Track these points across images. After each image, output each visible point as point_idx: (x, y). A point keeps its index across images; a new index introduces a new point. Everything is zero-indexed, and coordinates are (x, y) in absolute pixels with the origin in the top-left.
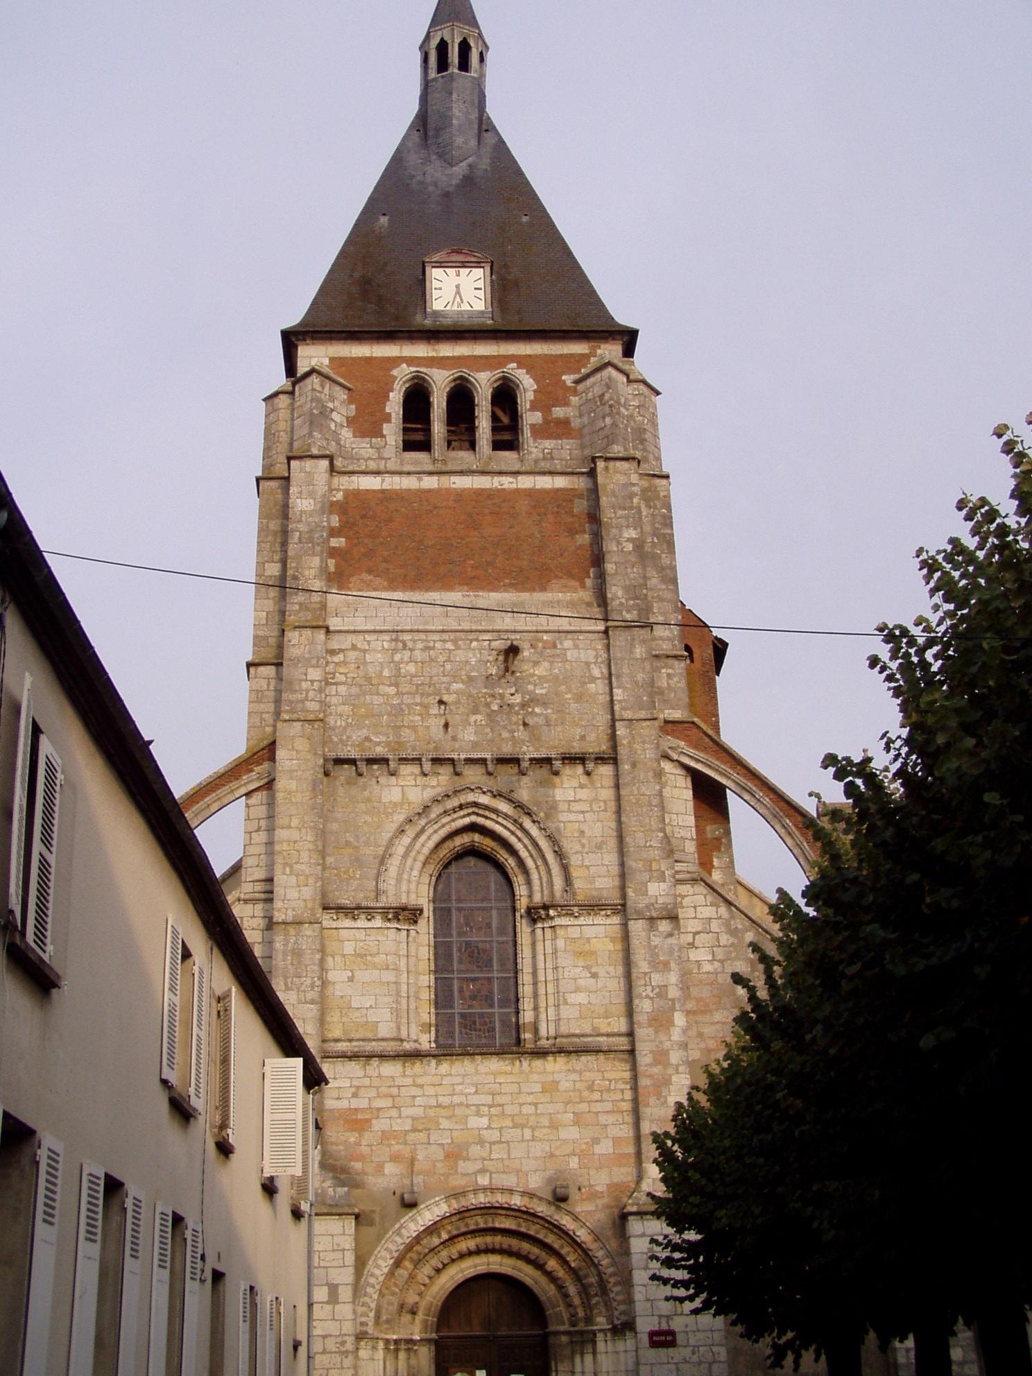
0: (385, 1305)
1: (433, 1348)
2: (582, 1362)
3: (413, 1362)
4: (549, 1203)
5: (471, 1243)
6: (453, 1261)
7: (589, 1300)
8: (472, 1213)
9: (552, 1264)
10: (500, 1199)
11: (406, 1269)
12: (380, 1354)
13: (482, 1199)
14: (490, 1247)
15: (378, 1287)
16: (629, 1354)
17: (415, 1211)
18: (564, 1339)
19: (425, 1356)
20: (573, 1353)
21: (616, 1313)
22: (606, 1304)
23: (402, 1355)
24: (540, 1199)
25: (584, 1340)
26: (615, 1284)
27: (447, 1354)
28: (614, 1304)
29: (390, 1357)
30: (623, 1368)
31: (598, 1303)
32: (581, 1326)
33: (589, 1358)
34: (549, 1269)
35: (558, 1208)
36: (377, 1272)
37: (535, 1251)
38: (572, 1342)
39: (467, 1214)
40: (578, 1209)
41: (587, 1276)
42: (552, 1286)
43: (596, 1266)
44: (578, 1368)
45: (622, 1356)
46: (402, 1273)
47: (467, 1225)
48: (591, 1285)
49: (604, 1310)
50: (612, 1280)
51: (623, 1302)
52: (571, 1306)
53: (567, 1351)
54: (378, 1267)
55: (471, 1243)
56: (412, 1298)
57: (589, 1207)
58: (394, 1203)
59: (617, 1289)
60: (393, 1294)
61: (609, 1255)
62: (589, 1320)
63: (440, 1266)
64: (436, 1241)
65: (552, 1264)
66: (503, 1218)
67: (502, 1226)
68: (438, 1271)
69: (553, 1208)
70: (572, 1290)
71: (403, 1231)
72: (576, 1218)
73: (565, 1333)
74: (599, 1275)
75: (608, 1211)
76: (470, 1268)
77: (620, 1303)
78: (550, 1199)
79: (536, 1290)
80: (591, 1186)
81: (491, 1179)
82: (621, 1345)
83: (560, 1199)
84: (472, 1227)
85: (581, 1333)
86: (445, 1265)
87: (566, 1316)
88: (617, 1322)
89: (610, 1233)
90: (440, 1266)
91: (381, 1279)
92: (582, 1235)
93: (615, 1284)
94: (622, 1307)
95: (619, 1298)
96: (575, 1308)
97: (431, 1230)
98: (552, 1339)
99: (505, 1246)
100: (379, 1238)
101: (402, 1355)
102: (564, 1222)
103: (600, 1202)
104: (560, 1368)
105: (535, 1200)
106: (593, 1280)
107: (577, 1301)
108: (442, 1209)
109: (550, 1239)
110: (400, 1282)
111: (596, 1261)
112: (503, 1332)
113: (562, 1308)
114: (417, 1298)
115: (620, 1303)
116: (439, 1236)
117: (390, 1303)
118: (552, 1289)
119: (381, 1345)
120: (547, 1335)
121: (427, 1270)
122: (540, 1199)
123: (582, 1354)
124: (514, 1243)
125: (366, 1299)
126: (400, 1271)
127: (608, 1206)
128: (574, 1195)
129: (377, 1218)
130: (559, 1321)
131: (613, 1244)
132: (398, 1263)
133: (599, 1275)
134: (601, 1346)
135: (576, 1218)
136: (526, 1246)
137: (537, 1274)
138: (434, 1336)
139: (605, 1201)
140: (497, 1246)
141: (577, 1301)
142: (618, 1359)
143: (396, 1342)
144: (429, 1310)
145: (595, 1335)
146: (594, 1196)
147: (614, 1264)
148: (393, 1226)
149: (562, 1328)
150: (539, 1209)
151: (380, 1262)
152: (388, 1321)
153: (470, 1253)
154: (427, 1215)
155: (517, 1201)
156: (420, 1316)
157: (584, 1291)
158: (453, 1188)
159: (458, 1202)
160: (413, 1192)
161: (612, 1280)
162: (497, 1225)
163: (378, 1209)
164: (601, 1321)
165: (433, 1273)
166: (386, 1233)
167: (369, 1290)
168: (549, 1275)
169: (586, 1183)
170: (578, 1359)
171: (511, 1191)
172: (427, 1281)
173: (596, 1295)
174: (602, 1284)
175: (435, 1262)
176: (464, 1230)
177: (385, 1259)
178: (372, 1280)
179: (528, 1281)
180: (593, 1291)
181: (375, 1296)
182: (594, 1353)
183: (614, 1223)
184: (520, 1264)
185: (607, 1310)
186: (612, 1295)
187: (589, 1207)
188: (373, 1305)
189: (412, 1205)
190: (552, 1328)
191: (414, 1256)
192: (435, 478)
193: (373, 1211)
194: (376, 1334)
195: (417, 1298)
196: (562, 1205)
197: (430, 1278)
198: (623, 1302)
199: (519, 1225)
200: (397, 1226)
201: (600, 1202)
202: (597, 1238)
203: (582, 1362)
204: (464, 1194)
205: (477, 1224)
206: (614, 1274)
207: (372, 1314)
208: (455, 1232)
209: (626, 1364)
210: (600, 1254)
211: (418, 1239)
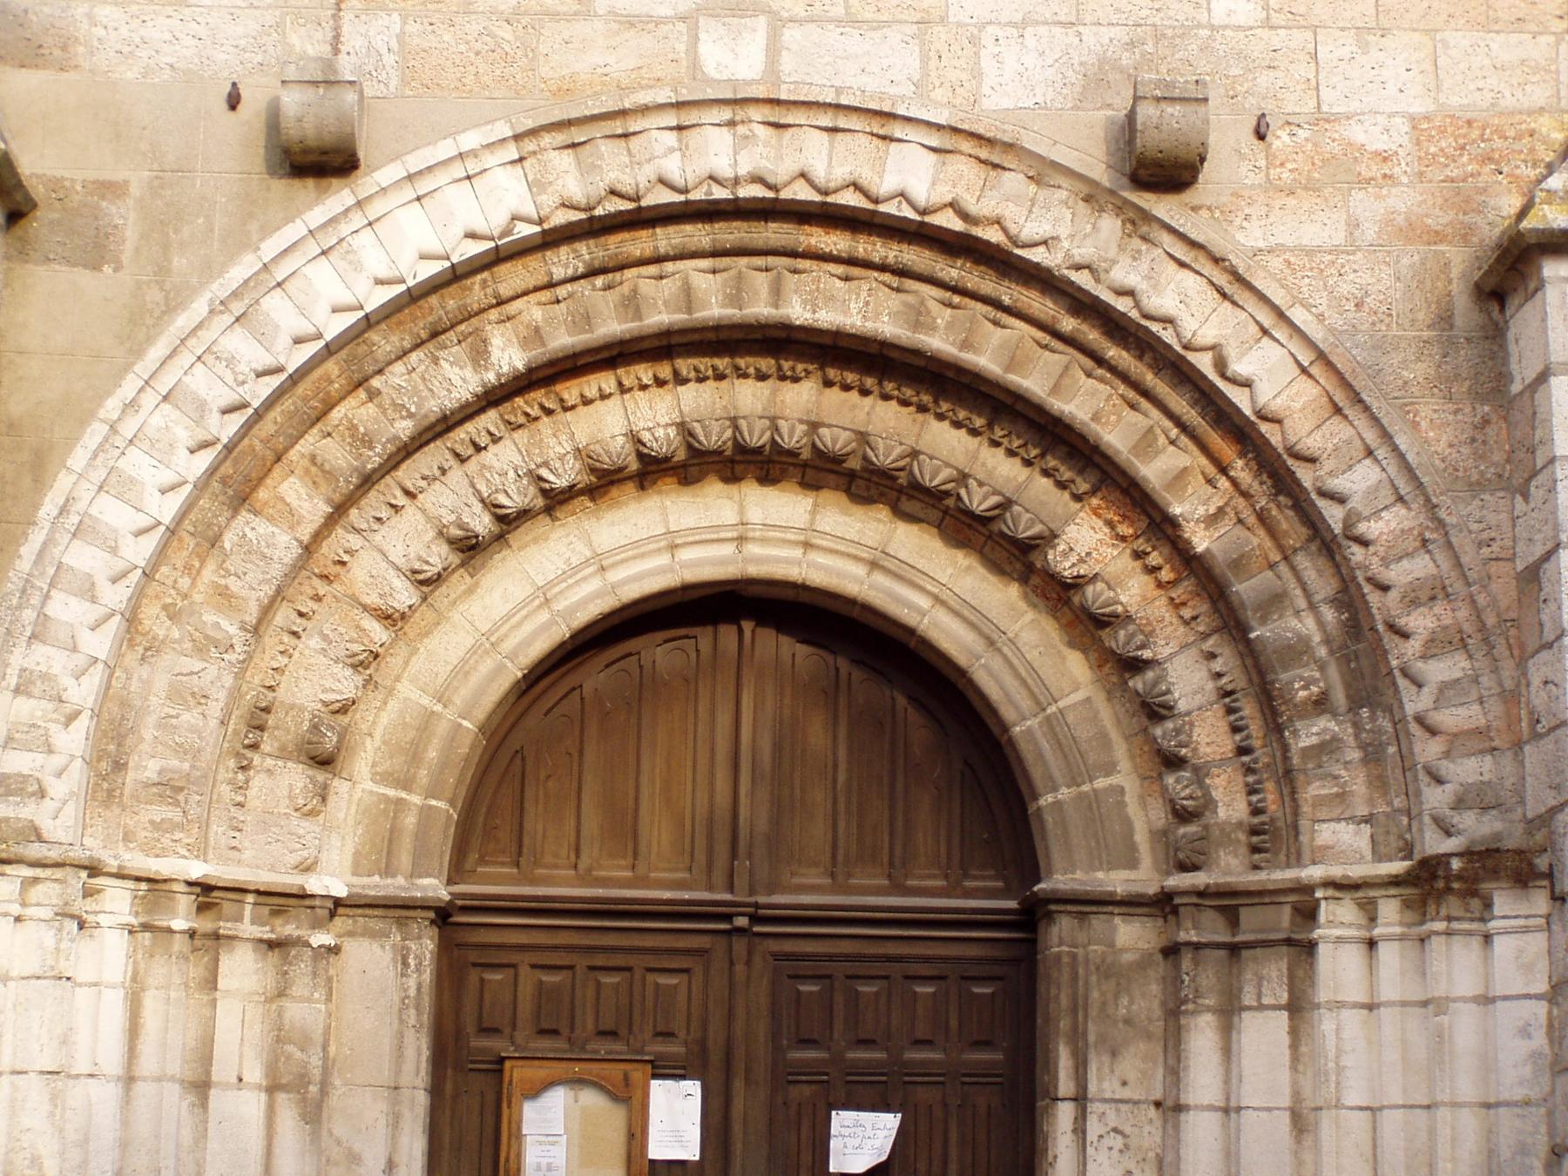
0: (157, 704)
1: (425, 945)
2: (1227, 1052)
3: (304, 1011)
4: (1093, 195)
5: (647, 412)
6: (555, 501)
7: (1276, 729)
8: (666, 238)
9: (1087, 540)
10: (818, 162)
11: (290, 517)
12: (108, 953)
13: (718, 158)
14: (756, 436)
15: (116, 596)
16: (1510, 1015)
17: (340, 196)
18: (1132, 936)
19: (377, 994)
20: (1175, 1013)
21: (1436, 798)
22: (1372, 755)
23: (242, 970)
24: (1043, 171)
25: (1238, 932)
26: (1436, 646)
27: (506, 995)
28: (1428, 750)
29: (169, 978)
30: (1467, 1087)
31: (1328, 747)
32: (1229, 868)
33: (1264, 1033)
34: (1066, 567)
35: (1139, 223)
36: (114, 514)
37: (994, 469)
38: (1171, 951)
39: (639, 243)
40: (1244, 238)
41: (1274, 602)
42: (1077, 666)
43: (1326, 544)
44: (1203, 1080)
45: (1465, 1025)
46: (266, 540)
47: (632, 305)
48: (1297, 651)
49: (1359, 785)
50: (1420, 622)
51: (1479, 740)
52: (1173, 762)
53: (1146, 1000)
54: (114, 484)
55: (647, 412)
56: (313, 680)
57: (1315, 228)
58: (234, 146)
59: (1440, 670)
60: (205, 645)
61: (1410, 486)
62: (1269, 836)
63: (482, 523)
64: (455, 379)
65: (1087, 540)
66: (826, 277)
67: (827, 318)
68: (470, 549)
69: (1110, 225)
70: (1187, 678)
71: (274, 304)
72: (1234, 283)
73: (1132, 904)
74: (1349, 598)
75: (1410, 257)
76: (637, 550)
77: (1458, 743)
78: (1099, 171)
79: (992, 679)
80: (1322, 119)
81: (774, 49)
82: (1457, 965)
83: (1159, 172)
84: (660, 317)
85: (1228, 902)
86: (508, 522)
87: (1144, 818)
88: (1434, 844)
89: (1418, 372)
90: (482, 523)
91: (140, 551)
92: (1268, 379)
93: (1436, 646)
94: (1469, 770)
95: (1452, 718)
96: (1201, 774)
97: (433, 306)
98: (1060, 935)
99: (835, 439)
100: (139, 326)
101: (242, 970)
102: (1163, 301)
103: (1365, 205)
104: (1101, 1083)
105: (1013, 181)
106: (1303, 625)
107: (1209, 737)
108: (504, 200)
109: (1085, 401)
110: (253, 588)
111: (1334, 515)
112: (808, 890)
113: (1125, 777)
114: (346, 684)
115: (1458, 743)
116: (479, 355)
117: (186, 695)
118: (1072, 677)
119: (118, 902)
120: (1033, 915)
121: (400, 539)
122: (1043, 171)
123: (1229, 1012)
124: (886, 424)
125: (43, 657)
126: (248, 528)
127: (1412, 231)
128: (1229, 165)
129: (126, 218)
130: (1103, 825)
131: (1434, 431)
132: (238, 479)
133: (1349, 598)
134: (1339, 967)
135: (1234, 283)
136: (946, 446)
137: (1001, 599)
138: (434, 887)
139: (1403, 200)
140: (793, 437)
141: (1209, 737)
142: (1440, 1041)
143: (206, 893)
144: (414, 755)
145: (1308, 914)
146: (1345, 171)
147: (1435, 533)
148: (210, 271)
149: (1118, 881)
150: (1030, 230)
151: (137, 463)
152: (169, 789)
153: (652, 470)
154: (403, 231)
155: (911, 178)
156: (360, 785)
157: (1259, 688)
158: (563, 92)
159: (585, 170)
160: (330, 83)
161: (1420, 622)
162: (798, 312)
163: (137, 179)
164: (1342, 844)
165: (438, 556)
166: (172, 307)
167: (66, 609)
168: (1060, 596)
169: (1297, 103)
170: (1202, 1036)
171: (884, 121)
172: (404, 595)
173: (1321, 704)
174: (1360, 634)
175: (451, 496)
176: (612, 327)
177: (160, 451)
178: (83, 558)
179: (949, 635)
180: (1300, 683)
181: (100, 644)
182: (1298, 1007)
183: (1445, 320)
184: (914, 544)
185: (1379, 783)
186: (1415, 702)
187: (1315, 228)
188: (83, 692)
189: (321, 161)
190: (1060, 879)
191: (337, 454)
192: (1016, 683)
193: (111, 189)
194: (93, 847)
195: (346, 684)
196: (1162, 206)
197: (427, 583)
198: (1479, 740)
199: (918, 318)
200: (239, 272)
201: (1371, 209)
202: (1347, 397)
203: (1227, 1052)
204: (619, 121)
205: (688, 296)
206: (1430, 593)
207: (74, 740)
208: (563, 340)
209: (1487, 1065)
210: (1360, 480)
211: (352, 355)
